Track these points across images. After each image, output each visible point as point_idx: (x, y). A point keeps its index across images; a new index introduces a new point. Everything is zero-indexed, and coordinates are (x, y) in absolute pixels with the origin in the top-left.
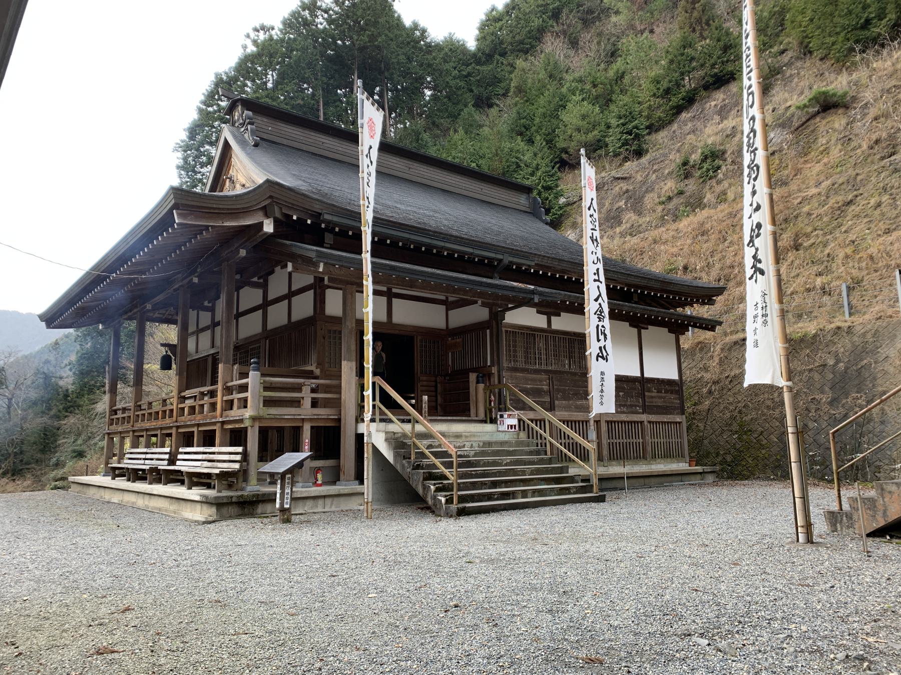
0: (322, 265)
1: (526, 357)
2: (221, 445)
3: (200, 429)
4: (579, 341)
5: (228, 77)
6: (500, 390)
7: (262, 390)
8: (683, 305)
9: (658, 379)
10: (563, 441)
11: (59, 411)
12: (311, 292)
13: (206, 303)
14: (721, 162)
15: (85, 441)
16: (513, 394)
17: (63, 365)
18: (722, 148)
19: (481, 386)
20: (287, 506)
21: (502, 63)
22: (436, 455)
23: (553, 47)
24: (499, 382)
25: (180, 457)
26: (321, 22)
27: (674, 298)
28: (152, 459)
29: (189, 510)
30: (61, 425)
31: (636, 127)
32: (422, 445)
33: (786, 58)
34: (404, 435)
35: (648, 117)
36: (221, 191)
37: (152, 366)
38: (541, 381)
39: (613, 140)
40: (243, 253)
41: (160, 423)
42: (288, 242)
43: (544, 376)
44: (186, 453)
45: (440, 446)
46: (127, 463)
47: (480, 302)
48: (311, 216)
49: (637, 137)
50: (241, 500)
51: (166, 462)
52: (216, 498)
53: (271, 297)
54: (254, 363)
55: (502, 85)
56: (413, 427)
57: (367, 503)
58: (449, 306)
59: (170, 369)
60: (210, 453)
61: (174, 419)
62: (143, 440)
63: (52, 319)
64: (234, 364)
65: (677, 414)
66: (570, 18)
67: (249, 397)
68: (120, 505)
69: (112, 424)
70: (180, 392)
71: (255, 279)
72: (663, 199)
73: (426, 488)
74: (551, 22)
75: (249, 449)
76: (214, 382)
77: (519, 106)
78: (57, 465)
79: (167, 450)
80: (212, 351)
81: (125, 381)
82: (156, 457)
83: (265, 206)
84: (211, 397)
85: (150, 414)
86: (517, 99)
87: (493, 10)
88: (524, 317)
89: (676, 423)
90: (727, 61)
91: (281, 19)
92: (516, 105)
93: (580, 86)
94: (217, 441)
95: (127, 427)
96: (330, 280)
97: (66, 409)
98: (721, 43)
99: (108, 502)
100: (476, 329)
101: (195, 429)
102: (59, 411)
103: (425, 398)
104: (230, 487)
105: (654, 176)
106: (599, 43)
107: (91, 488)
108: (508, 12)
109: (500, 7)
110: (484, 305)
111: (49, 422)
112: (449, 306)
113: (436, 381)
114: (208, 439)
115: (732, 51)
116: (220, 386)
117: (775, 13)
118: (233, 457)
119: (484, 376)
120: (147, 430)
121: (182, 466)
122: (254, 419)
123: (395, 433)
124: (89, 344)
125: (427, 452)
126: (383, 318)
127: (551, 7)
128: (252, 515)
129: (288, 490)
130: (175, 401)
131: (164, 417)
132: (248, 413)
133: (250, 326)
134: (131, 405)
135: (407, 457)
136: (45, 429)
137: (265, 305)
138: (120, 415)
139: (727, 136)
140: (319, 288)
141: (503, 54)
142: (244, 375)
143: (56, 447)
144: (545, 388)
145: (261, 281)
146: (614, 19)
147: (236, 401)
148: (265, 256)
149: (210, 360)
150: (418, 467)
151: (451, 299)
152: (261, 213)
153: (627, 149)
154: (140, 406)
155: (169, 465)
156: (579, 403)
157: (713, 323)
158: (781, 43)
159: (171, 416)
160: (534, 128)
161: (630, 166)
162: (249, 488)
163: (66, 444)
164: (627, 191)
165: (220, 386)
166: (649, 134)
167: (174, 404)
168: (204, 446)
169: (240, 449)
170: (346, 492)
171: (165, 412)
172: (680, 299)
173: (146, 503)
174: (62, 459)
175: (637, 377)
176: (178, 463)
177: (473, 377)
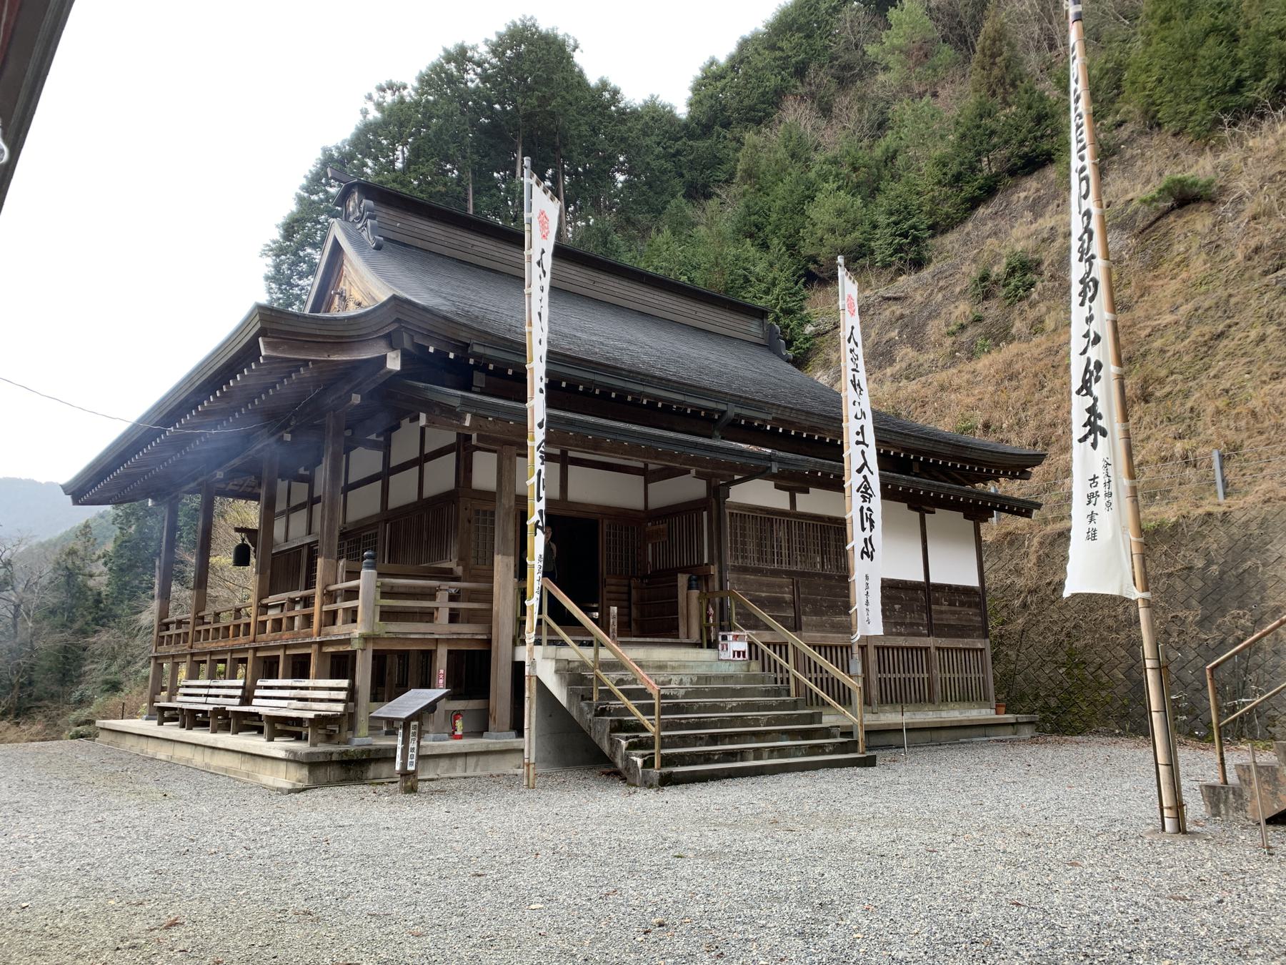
0: (468, 417)
4: (837, 528)
8: (985, 480)
9: (950, 586)
14: (1035, 277)
15: (122, 668)
16: (740, 605)
17: (95, 557)
18: (1036, 256)
19: (695, 593)
20: (411, 768)
21: (725, 137)
22: (629, 694)
24: (721, 588)
25: (257, 692)
26: (472, 79)
27: (972, 469)
28: (217, 696)
30: (89, 643)
31: (914, 227)
32: (609, 679)
33: (1124, 133)
34: (583, 665)
35: (931, 214)
37: (222, 559)
38: (781, 586)
43: (786, 580)
45: (635, 681)
46: (181, 702)
47: (693, 472)
49: (916, 240)
50: (345, 758)
51: (237, 701)
55: (724, 167)
56: (597, 653)
57: (528, 765)
58: (650, 476)
61: (251, 637)
63: (81, 491)
64: (340, 558)
65: (978, 637)
66: (820, 76)
67: (361, 608)
68: (170, 764)
69: (161, 644)
70: (260, 599)
71: (373, 437)
73: (614, 744)
74: (793, 82)
76: (310, 584)
77: (748, 196)
78: (81, 702)
79: (240, 682)
80: (308, 540)
82: (223, 693)
84: (305, 606)
85: (217, 630)
87: (712, 64)
88: (757, 494)
89: (977, 650)
90: (1042, 136)
91: (417, 74)
94: (312, 671)
95: (183, 648)
96: (480, 438)
97: (96, 620)
98: (1033, 112)
99: (152, 759)
100: (688, 510)
101: (281, 653)
103: (614, 610)
104: (329, 738)
105: (940, 295)
106: (860, 110)
108: (733, 67)
109: (722, 59)
110: (699, 475)
111: (72, 640)
112: (650, 476)
114: (300, 668)
115: (1048, 122)
116: (318, 591)
118: (334, 695)
119: (700, 578)
120: (211, 653)
123: (569, 662)
125: (616, 689)
126: (556, 494)
127: (793, 60)
128: (360, 780)
129: (413, 745)
130: (253, 611)
131: (236, 635)
132: (358, 630)
133: (364, 504)
134: (190, 616)
135: (586, 697)
136: (66, 649)
138: (173, 630)
139: (1043, 241)
140: (463, 450)
141: (726, 125)
143: (80, 676)
144: (788, 597)
146: (881, 77)
147: (340, 613)
149: (305, 552)
150: (603, 712)
151: (651, 467)
152: (383, 344)
153: (901, 258)
154: (203, 618)
155: (241, 704)
158: (1117, 112)
159: (247, 633)
160: (769, 228)
162: (357, 741)
163: (95, 671)
164: (902, 316)
166: (932, 236)
169: (344, 683)
170: (497, 747)
171: (238, 626)
173: (207, 760)
174: (89, 693)
175: (919, 583)
176: (255, 701)
177: (682, 580)
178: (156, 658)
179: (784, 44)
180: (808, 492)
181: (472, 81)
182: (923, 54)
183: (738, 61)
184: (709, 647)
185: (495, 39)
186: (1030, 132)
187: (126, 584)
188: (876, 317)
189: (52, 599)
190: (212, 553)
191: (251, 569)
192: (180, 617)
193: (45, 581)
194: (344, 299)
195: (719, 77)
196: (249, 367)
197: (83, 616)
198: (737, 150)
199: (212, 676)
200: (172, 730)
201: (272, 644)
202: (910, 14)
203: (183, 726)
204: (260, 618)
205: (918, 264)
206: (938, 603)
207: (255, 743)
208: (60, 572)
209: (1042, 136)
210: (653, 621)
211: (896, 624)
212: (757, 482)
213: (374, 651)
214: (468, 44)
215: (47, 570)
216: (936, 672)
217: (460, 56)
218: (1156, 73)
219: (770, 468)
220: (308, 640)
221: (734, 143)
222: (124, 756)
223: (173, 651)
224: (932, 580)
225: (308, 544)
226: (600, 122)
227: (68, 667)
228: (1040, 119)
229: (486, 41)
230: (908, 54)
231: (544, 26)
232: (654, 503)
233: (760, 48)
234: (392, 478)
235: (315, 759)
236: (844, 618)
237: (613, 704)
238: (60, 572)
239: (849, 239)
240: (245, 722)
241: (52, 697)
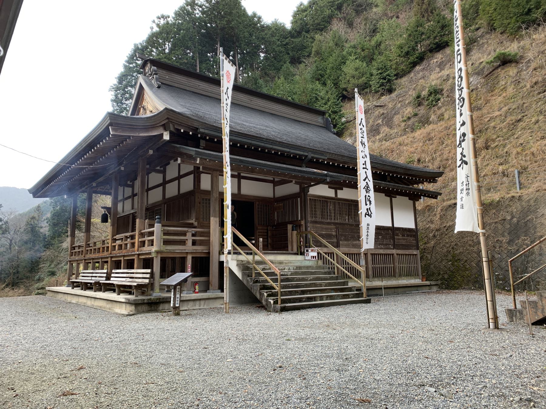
0: (198, 159)
1: (322, 215)
2: (138, 268)
4: (354, 205)
5: (142, 46)
8: (418, 183)
9: (402, 228)
10: (345, 266)
12: (192, 176)
13: (129, 183)
15: (56, 266)
16: (314, 237)
19: (295, 232)
21: (307, 37)
22: (268, 274)
23: (338, 27)
24: (306, 230)
25: (113, 275)
26: (198, 13)
27: (412, 179)
28: (96, 277)
29: (118, 308)
31: (388, 75)
32: (259, 268)
33: (479, 33)
34: (248, 262)
35: (396, 69)
36: (138, 115)
38: (331, 229)
40: (151, 152)
41: (101, 255)
44: (116, 273)
46: (81, 279)
47: (294, 181)
49: (389, 81)
50: (150, 302)
51: (104, 279)
52: (134, 300)
54: (158, 218)
55: (307, 50)
56: (254, 257)
58: (275, 184)
60: (131, 273)
64: (146, 219)
65: (415, 249)
66: (348, 9)
67: (155, 239)
68: (77, 304)
69: (72, 255)
70: (113, 236)
71: (158, 168)
72: (405, 118)
73: (261, 295)
74: (336, 12)
75: (154, 270)
76: (133, 230)
77: (317, 63)
78: (39, 280)
79: (105, 271)
84: (132, 239)
85: (95, 249)
86: (316, 58)
87: (301, 5)
88: (321, 190)
89: (414, 255)
90: (444, 35)
91: (174, 11)
93: (354, 50)
94: (135, 266)
96: (203, 168)
98: (440, 24)
99: (70, 303)
101: (122, 259)
103: (261, 239)
104: (143, 293)
106: (365, 24)
107: (59, 294)
110: (296, 183)
112: (275, 184)
113: (267, 229)
114: (130, 265)
116: (137, 233)
118: (145, 276)
119: (297, 226)
120: (93, 259)
122: (157, 252)
123: (242, 261)
125: (262, 272)
126: (236, 192)
128: (156, 311)
129: (178, 296)
130: (110, 241)
131: (103, 251)
132: (154, 249)
133: (155, 196)
134: (83, 244)
135: (250, 275)
138: (77, 250)
139: (444, 80)
140: (197, 173)
141: (308, 32)
142: (152, 226)
144: (334, 233)
145: (162, 169)
146: (374, 10)
147: (146, 242)
148: (163, 155)
151: (276, 180)
152: (162, 128)
153: (383, 89)
154: (89, 244)
155: (106, 280)
156: (355, 242)
157: (436, 194)
158: (477, 24)
159: (107, 251)
160: (326, 76)
164: (383, 114)
166: (396, 79)
167: (109, 243)
169: (149, 271)
170: (213, 296)
171: (104, 248)
172: (416, 179)
173: (93, 303)
174: (42, 276)
176: (112, 279)
177: (290, 227)
178: (70, 261)
187: (56, 231)
189: (25, 238)
191: (109, 224)
192: (79, 244)
194: (145, 109)
195: (305, 10)
196: (105, 139)
199: (94, 268)
205: (390, 91)
206: (397, 235)
210: (278, 244)
211: (380, 244)
213: (193, 257)
216: (397, 264)
219: (326, 179)
221: (311, 40)
223: (77, 258)
224: (395, 226)
236: (357, 242)
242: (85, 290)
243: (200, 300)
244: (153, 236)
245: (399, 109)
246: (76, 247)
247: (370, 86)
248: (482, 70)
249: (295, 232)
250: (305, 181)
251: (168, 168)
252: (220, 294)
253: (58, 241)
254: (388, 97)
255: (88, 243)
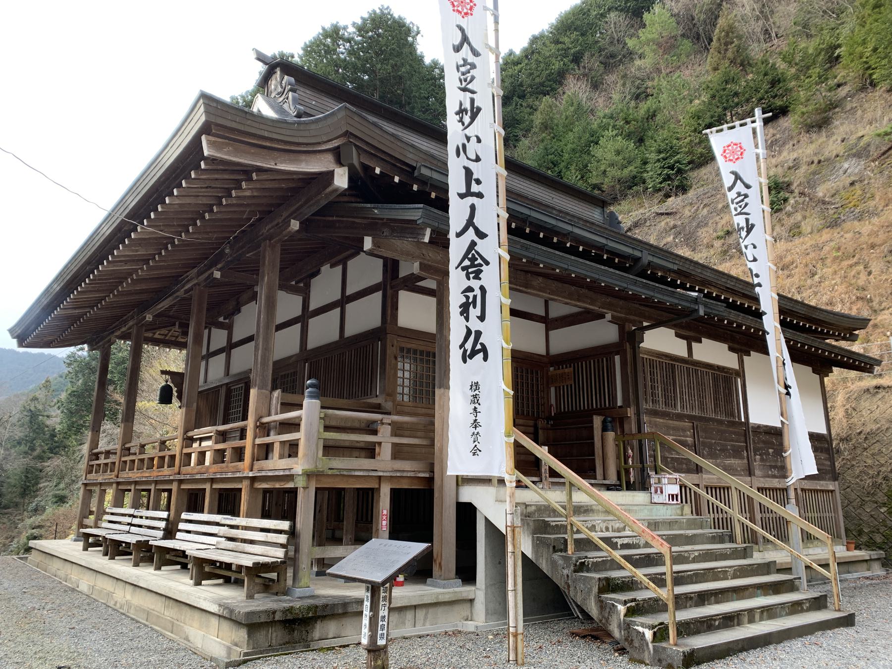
1: (666, 397)
2: (249, 515)
3: (215, 486)
5: (244, 101)
6: (640, 441)
7: (322, 430)
11: (44, 452)
12: (378, 295)
13: (221, 319)
14: (787, 195)
15: (68, 485)
17: (53, 404)
18: (786, 179)
19: (611, 435)
20: (381, 642)
21: (521, 105)
23: (575, 89)
24: (639, 431)
25: (182, 526)
26: (342, 49)
28: (140, 526)
29: (196, 624)
30: (44, 467)
31: (678, 162)
33: (843, 92)
34: (549, 510)
35: (690, 153)
37: (148, 403)
38: (684, 430)
39: (652, 175)
40: (295, 225)
41: (154, 474)
42: (369, 205)
43: (687, 424)
44: (190, 521)
46: (105, 531)
47: (609, 316)
48: (401, 172)
49: (680, 171)
50: (289, 617)
51: (160, 534)
52: (249, 614)
53: (313, 306)
54: (311, 386)
55: (521, 126)
57: (516, 635)
59: (170, 402)
60: (232, 527)
61: (176, 468)
62: (128, 498)
64: (274, 388)
65: (829, 480)
66: (591, 62)
67: (302, 442)
68: (90, 601)
69: (90, 472)
70: (186, 432)
72: (721, 233)
73: (606, 608)
74: (571, 66)
75: (299, 526)
76: (245, 418)
77: (545, 142)
78: (36, 511)
79: (164, 515)
80: (226, 381)
81: (113, 418)
82: (146, 525)
83: (338, 147)
85: (142, 460)
86: (544, 135)
87: (510, 55)
89: (828, 491)
90: (776, 96)
91: (302, 45)
92: (542, 141)
93: (612, 122)
94: (243, 507)
95: (109, 476)
97: (51, 450)
98: (769, 78)
99: (73, 590)
100: (603, 352)
101: (207, 486)
102: (44, 452)
104: (267, 587)
105: (705, 210)
106: (624, 85)
107: (55, 559)
108: (526, 56)
109: (518, 51)
111: (32, 463)
112: (550, 323)
114: (227, 503)
115: (781, 85)
116: (250, 423)
117: (822, 50)
118: (272, 537)
119: (615, 420)
120: (136, 483)
121: (188, 542)
122: (309, 475)
123: (527, 506)
124: (81, 381)
127: (572, 51)
128: (306, 645)
130: (178, 442)
131: (161, 466)
132: (298, 466)
133: (286, 344)
134: (116, 446)
135: (560, 547)
136: (27, 471)
137: (303, 319)
138: (102, 461)
139: (789, 168)
141: (522, 97)
143: (37, 490)
144: (690, 440)
146: (638, 62)
147: (277, 447)
149: (223, 392)
150: (581, 567)
152: (330, 157)
153: (669, 185)
154: (129, 449)
155: (165, 538)
157: (872, 362)
158: (835, 77)
159: (171, 464)
160: (563, 164)
161: (673, 202)
162: (298, 592)
163: (47, 488)
164: (675, 227)
165: (250, 423)
166: (692, 169)
167: (176, 447)
168: (219, 512)
169: (285, 525)
170: (446, 598)
171: (162, 458)
173: (128, 597)
174: (42, 503)
176: (179, 535)
177: (597, 421)
178: (86, 485)
179: (566, 40)
180: (700, 342)
181: (343, 53)
182: (668, 46)
183: (528, 53)
184: (628, 489)
185: (359, 22)
186: (767, 92)
187: (73, 423)
188: (652, 228)
189: (19, 434)
190: (138, 399)
191: (176, 402)
192: (107, 448)
193: (14, 420)
195: (517, 63)
197: (41, 445)
198: (530, 114)
199: (136, 505)
200: (96, 559)
201: (198, 477)
202: (658, 18)
203: (106, 554)
204: (186, 451)
205: (683, 189)
207: (177, 583)
208: (25, 413)
209: (776, 96)
211: (771, 467)
212: (662, 330)
213: (317, 489)
214: (342, 24)
215: (16, 411)
217: (335, 33)
218: (870, 46)
219: (697, 311)
220: (238, 475)
221: (528, 109)
222: (47, 583)
223: (100, 480)
225: (227, 384)
226: (433, 90)
227: (29, 485)
228: (774, 83)
229: (354, 24)
230: (659, 45)
231: (397, 13)
232: (555, 349)
233: (548, 42)
234: (311, 321)
235: (256, 620)
237: (593, 556)
238: (25, 413)
239: (626, 172)
240: (168, 556)
241: (17, 505)
242: (112, 558)
243: (415, 607)
244: (299, 431)
245: (705, 217)
246: (101, 453)
247: (644, 182)
248: (865, 149)
249: (611, 435)
250: (632, 317)
251: (316, 282)
252: (466, 591)
253: (76, 440)
254: (679, 199)
255: (127, 446)
